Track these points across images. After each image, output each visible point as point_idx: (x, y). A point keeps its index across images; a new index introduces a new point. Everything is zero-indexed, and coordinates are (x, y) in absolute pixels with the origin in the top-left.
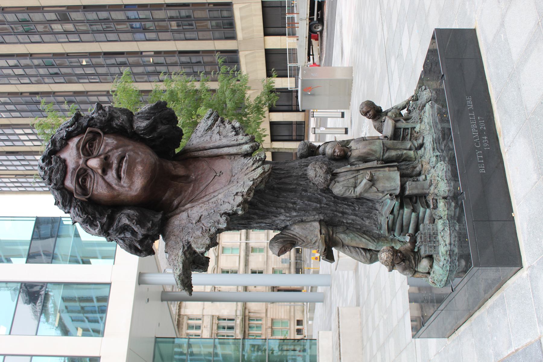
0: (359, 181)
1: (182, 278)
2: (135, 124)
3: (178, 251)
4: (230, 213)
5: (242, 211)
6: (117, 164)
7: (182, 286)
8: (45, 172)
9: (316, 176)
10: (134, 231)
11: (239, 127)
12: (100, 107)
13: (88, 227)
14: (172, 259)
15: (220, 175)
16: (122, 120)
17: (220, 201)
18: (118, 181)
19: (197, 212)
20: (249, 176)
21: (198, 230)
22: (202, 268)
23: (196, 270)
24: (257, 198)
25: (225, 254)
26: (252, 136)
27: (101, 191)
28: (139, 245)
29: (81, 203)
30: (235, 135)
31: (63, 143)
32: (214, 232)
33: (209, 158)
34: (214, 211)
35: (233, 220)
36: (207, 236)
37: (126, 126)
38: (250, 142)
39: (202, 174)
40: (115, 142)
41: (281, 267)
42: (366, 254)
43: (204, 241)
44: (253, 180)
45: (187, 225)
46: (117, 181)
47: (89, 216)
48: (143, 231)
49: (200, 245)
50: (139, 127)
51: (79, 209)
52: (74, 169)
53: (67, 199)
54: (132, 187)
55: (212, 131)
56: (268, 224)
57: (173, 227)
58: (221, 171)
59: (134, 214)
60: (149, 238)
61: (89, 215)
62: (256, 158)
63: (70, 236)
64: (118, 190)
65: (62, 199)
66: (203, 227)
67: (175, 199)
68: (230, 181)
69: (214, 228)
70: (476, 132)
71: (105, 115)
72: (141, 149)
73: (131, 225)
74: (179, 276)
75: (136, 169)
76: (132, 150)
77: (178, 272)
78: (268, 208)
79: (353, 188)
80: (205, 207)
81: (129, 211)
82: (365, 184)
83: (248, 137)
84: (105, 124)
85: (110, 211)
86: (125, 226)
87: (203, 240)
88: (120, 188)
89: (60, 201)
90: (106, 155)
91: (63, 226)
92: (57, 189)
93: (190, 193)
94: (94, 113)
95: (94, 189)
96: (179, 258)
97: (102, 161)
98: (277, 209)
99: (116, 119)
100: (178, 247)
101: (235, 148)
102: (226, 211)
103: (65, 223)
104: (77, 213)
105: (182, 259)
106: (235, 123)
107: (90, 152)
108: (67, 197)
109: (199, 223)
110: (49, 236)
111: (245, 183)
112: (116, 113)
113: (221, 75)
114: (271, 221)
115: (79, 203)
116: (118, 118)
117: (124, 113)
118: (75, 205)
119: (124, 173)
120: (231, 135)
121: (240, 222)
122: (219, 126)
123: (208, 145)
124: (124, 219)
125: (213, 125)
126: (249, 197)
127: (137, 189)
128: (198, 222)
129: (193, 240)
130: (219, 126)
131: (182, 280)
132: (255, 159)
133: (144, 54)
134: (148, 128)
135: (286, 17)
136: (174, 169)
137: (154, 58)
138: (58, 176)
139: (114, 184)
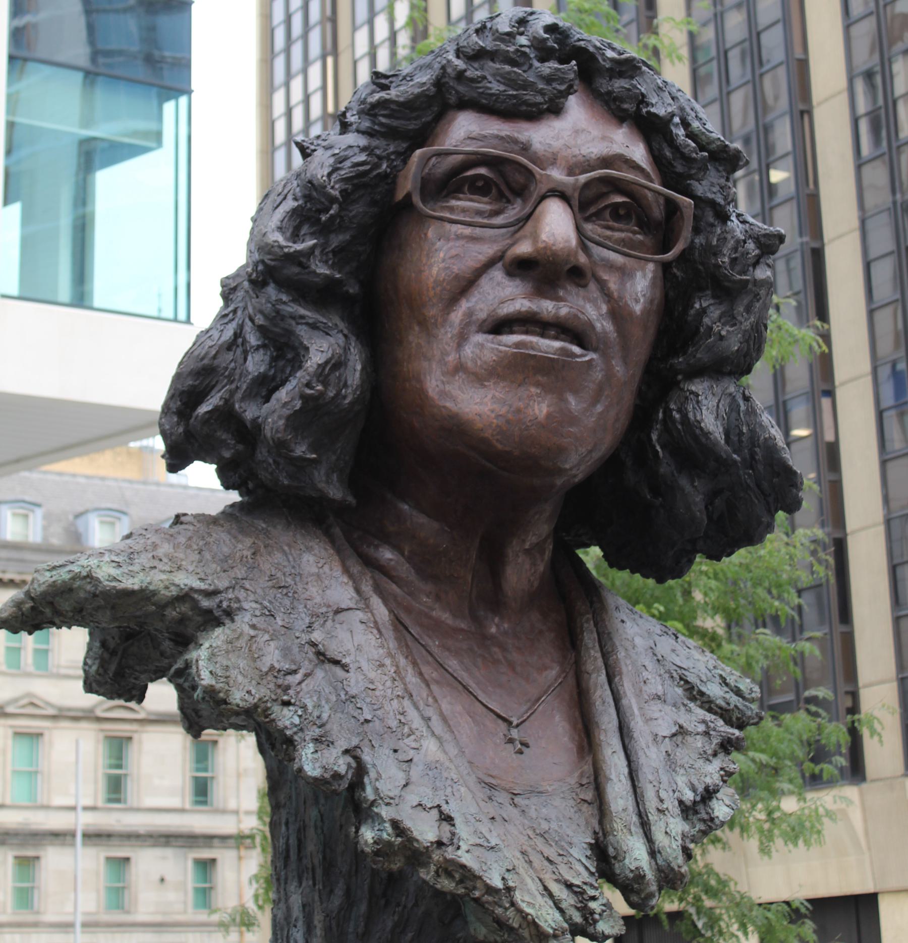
1: (80, 587)
2: (706, 384)
3: (191, 569)
4: (364, 789)
5: (375, 842)
6: (557, 317)
7: (43, 588)
10: (276, 389)
11: (712, 820)
12: (768, 246)
13: (290, 204)
14: (155, 546)
15: (511, 741)
16: (723, 333)
17: (414, 745)
18: (484, 321)
19: (359, 648)
20: (521, 871)
21: (286, 652)
22: (106, 671)
23: (98, 644)
25: (10, 742)
26: (683, 876)
27: (442, 255)
28: (216, 409)
30: (681, 802)
31: (626, 106)
32: (280, 724)
34: (367, 721)
35: (322, 801)
36: (261, 692)
37: (697, 351)
38: (659, 870)
39: (512, 666)
40: (638, 308)
43: (240, 678)
44: (509, 889)
45: (301, 608)
46: (482, 315)
48: (274, 422)
49: (225, 663)
50: (698, 402)
51: (361, 168)
52: (525, 148)
53: (403, 122)
54: (460, 377)
55: (686, 701)
57: (289, 546)
59: (345, 385)
60: (240, 447)
61: (340, 204)
62: (593, 898)
63: (87, 122)
64: (445, 321)
65: (401, 99)
66: (299, 677)
67: (403, 554)
68: (491, 787)
69: (297, 720)
71: (738, 268)
72: (613, 413)
73: (301, 376)
74: (89, 576)
75: (538, 395)
76: (609, 374)
77: (105, 572)
80: (384, 685)
81: (359, 367)
83: (680, 860)
84: (700, 267)
85: (353, 289)
86: (294, 348)
87: (245, 676)
89: (393, 94)
90: (589, 275)
91: (155, 102)
92: (439, 83)
93: (430, 617)
94: (744, 222)
95: (448, 226)
96: (163, 577)
97: (568, 255)
99: (723, 308)
100: (209, 571)
101: (630, 804)
102: (373, 774)
103: (169, 107)
104: (346, 159)
105: (162, 585)
107: (593, 210)
108: (409, 120)
109: (311, 655)
110: (100, 46)
111: (490, 856)
112: (748, 309)
113: (814, 726)
115: (384, 166)
116: (730, 318)
117: (747, 341)
118: (378, 152)
119: (518, 345)
120: (680, 783)
121: (311, 833)
122: (706, 734)
123: (627, 687)
124: (325, 346)
125: (708, 704)
126: (437, 872)
127: (454, 399)
128: (319, 654)
129: (241, 634)
130: (706, 734)
131: (71, 590)
132: (591, 892)
133: (826, 402)
134: (696, 438)
136: (527, 547)
137: (809, 443)
138: (496, 87)
139: (470, 305)
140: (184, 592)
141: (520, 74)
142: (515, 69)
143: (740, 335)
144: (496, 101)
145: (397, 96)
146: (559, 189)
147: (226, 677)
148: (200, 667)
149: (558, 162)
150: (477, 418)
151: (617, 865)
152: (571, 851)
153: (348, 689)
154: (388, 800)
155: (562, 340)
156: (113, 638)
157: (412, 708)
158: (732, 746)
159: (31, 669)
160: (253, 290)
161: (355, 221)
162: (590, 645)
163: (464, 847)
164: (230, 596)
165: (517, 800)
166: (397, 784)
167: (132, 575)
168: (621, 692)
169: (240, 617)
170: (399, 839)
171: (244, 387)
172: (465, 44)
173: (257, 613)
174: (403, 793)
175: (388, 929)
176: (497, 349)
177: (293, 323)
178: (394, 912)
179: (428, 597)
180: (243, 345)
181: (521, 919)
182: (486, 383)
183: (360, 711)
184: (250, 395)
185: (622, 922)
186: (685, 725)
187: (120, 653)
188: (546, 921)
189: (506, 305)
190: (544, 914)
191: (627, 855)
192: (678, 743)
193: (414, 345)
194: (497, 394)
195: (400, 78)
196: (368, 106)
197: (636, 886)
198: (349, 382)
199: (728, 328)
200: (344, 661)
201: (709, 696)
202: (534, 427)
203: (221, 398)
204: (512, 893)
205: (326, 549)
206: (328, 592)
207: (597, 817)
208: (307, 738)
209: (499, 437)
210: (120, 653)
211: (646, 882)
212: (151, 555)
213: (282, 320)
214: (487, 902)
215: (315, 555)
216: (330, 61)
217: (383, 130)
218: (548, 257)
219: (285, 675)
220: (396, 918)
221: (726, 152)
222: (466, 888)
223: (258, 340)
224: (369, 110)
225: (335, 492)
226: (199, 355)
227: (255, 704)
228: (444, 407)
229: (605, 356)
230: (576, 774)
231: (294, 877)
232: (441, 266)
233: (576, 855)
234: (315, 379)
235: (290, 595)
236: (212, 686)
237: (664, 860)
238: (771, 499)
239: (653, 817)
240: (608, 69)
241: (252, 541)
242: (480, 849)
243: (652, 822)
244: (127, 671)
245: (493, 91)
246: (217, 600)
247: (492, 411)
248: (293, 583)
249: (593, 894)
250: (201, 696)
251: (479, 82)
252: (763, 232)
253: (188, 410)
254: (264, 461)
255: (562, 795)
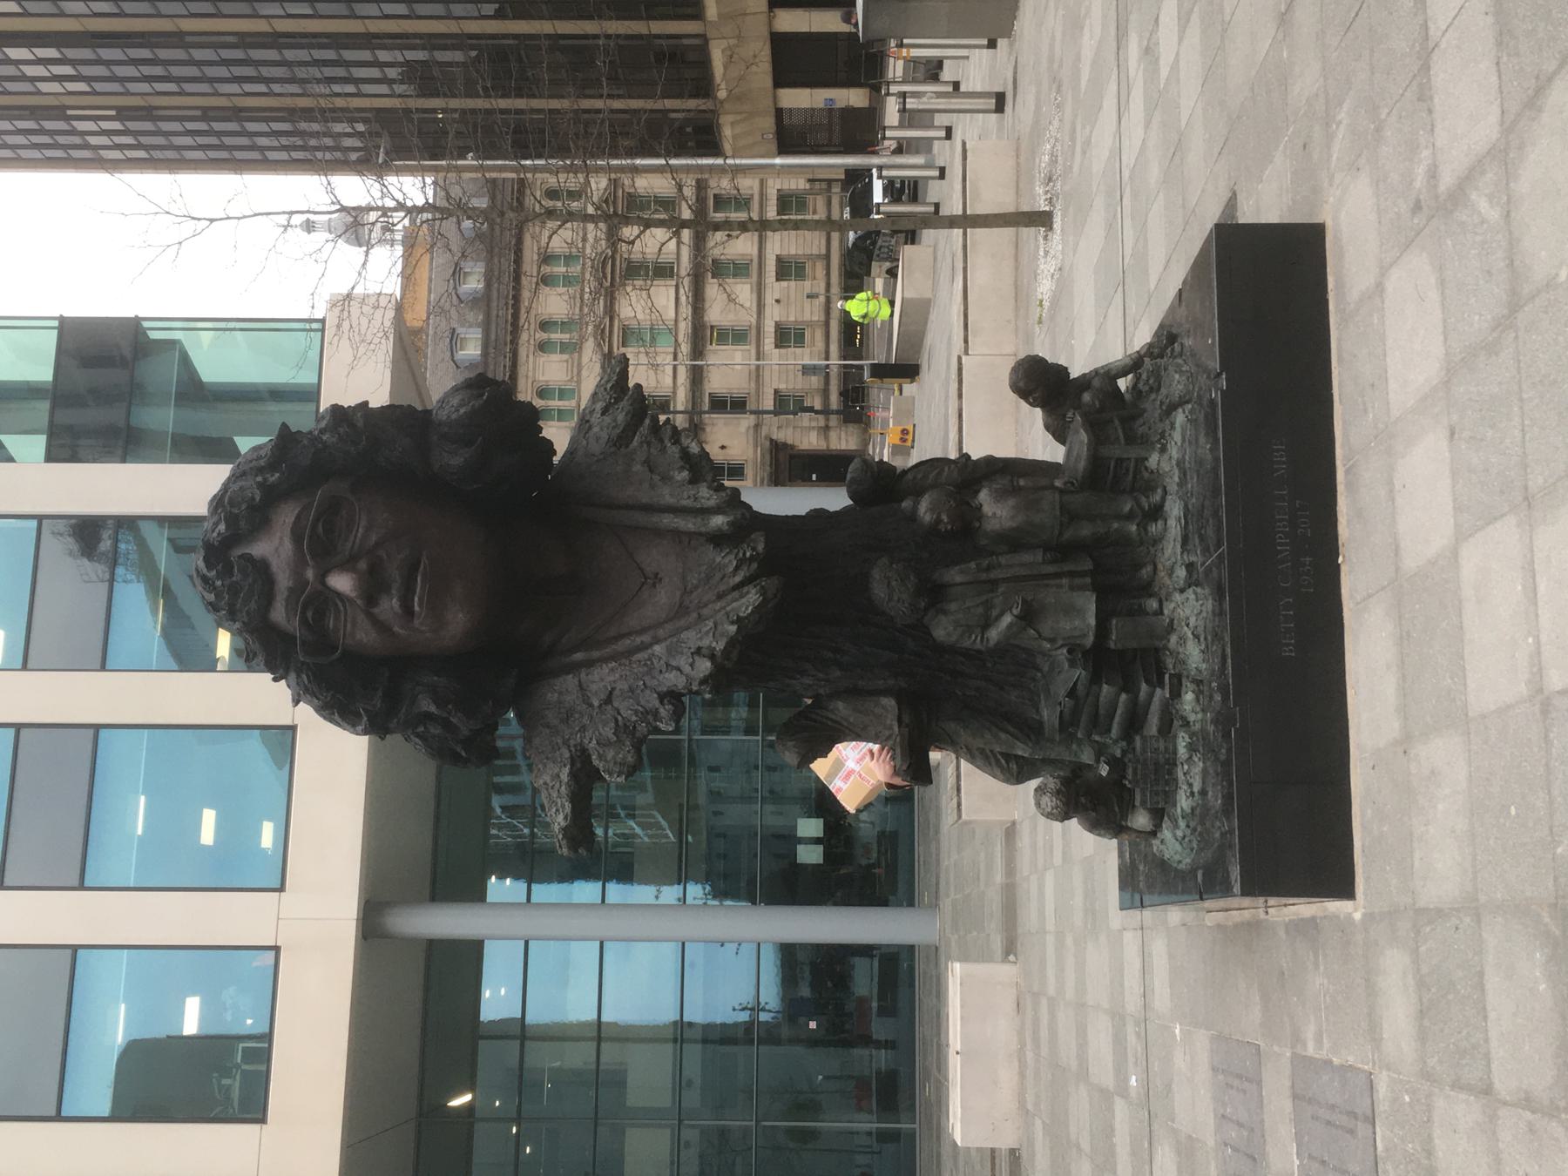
0: (995, 613)
9: (890, 600)
41: (799, 386)
42: (1008, 764)
58: (657, 574)
66: (620, 718)
70: (1286, 544)
79: (979, 630)
82: (1010, 626)
96: (563, 787)
106: (689, 441)
111: (720, 628)
119: (420, 605)
122: (649, 444)
132: (741, 555)
138: (253, 605)
159: (575, 335)
167: (563, 806)
216: (70, 112)
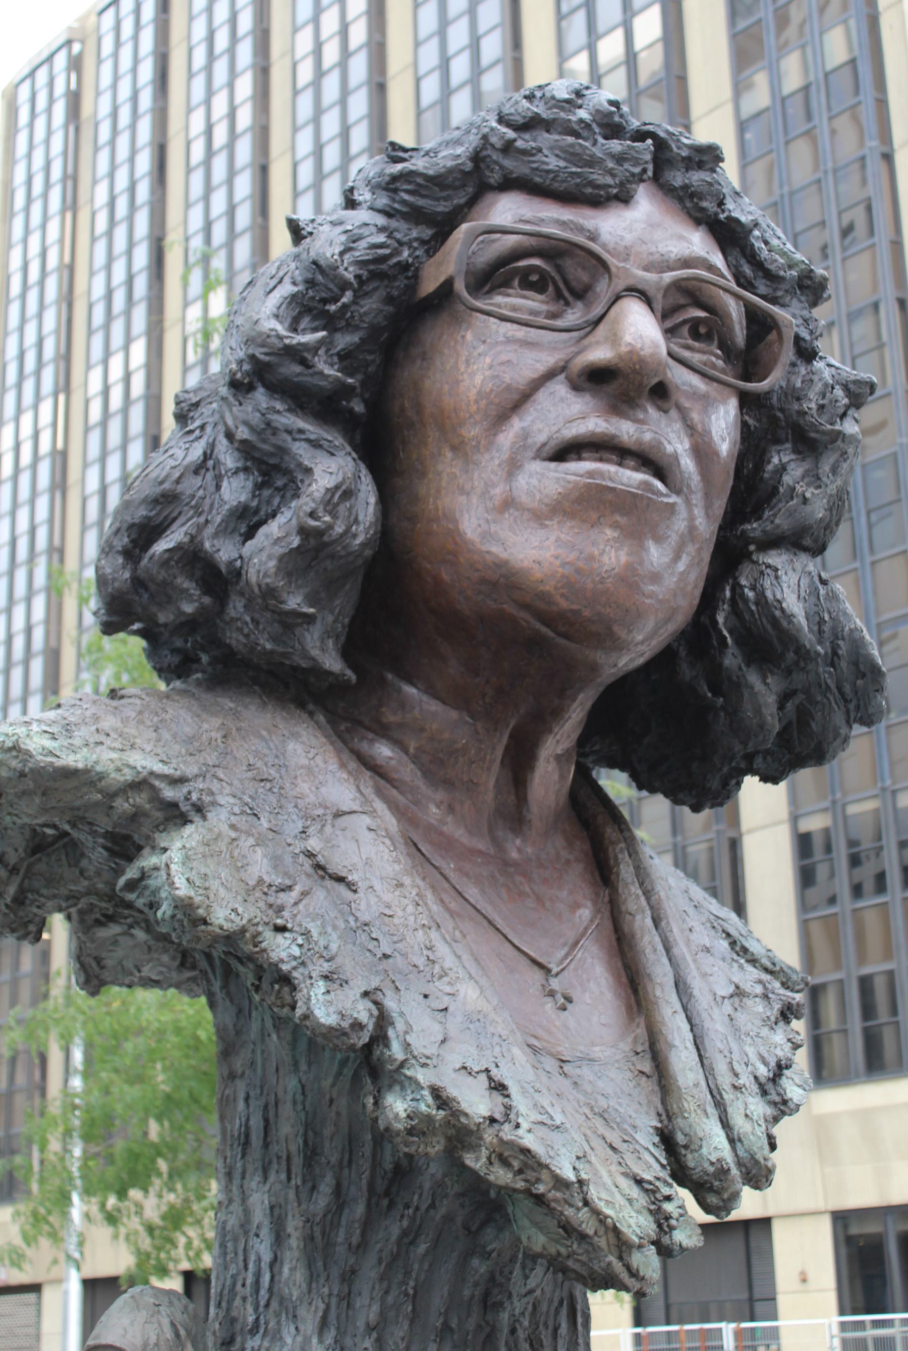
3: (148, 748)
4: (387, 1045)
5: (409, 1117)
6: (640, 442)
8: (568, 101)
13: (287, 289)
14: (96, 718)
15: (552, 994)
16: (808, 495)
17: (448, 989)
18: (544, 445)
21: (276, 862)
24: (442, 1211)
28: (178, 547)
29: (404, 267)
31: (705, 204)
32: (274, 956)
33: (613, 938)
34: (386, 956)
35: (303, 1067)
37: (775, 515)
43: (222, 892)
44: (581, 1182)
46: (541, 438)
47: (347, 297)
49: (203, 870)
50: (777, 577)
51: (381, 251)
54: (509, 517)
56: (266, 1278)
59: (356, 521)
60: (207, 600)
61: (355, 291)
64: (491, 444)
65: (431, 172)
66: (295, 894)
67: (406, 752)
69: (296, 951)
74: (15, 748)
78: (373, 1274)
84: (779, 414)
86: (287, 472)
88: (505, 455)
92: (477, 158)
93: (441, 833)
96: (114, 755)
98: (370, 1329)
99: (806, 465)
102: (400, 1025)
105: (112, 767)
108: (437, 199)
112: (834, 470)
114: (295, 1294)
115: (406, 254)
116: (815, 479)
118: (398, 235)
119: (591, 474)
120: (751, 1055)
121: (287, 1110)
124: (334, 468)
128: (318, 867)
129: (219, 835)
130: (766, 997)
132: (666, 1191)
134: (775, 622)
135: (722, 1325)
138: (553, 163)
140: (141, 776)
141: (586, 148)
142: (580, 141)
143: (825, 501)
144: (553, 179)
145: (425, 168)
146: (640, 287)
147: (206, 889)
148: (173, 873)
149: (632, 258)
150: (536, 566)
151: (689, 1157)
152: (638, 1137)
153: (358, 914)
154: (423, 1060)
155: (644, 472)
156: (16, 850)
157: (442, 942)
158: (792, 1013)
160: (234, 395)
161: (367, 320)
162: (629, 880)
163: (525, 1125)
164: (201, 786)
165: (567, 1068)
166: (433, 1039)
167: (73, 750)
168: (671, 939)
169: (213, 814)
170: (442, 1113)
171: (218, 519)
172: (512, 110)
173: (237, 810)
174: (441, 1052)
175: (394, 1238)
176: (564, 479)
177: (289, 438)
178: (402, 1216)
179: (438, 807)
180: (214, 468)
181: (597, 1224)
182: (547, 523)
183: (375, 943)
184: (224, 530)
185: (699, 1231)
186: (741, 984)
187: (22, 871)
188: (630, 1226)
189: (574, 424)
190: (627, 1216)
191: (704, 1143)
192: (736, 1006)
193: (445, 476)
194: (562, 536)
195: (422, 153)
196: (387, 179)
197: (716, 1183)
198: (361, 518)
199: (812, 489)
200: (350, 878)
201: (753, 954)
202: (610, 580)
203: (186, 534)
204: (585, 1188)
205: (315, 736)
206: (323, 790)
207: (659, 1095)
208: (314, 974)
209: (565, 591)
210: (22, 871)
211: (730, 1178)
212: (94, 728)
213: (274, 434)
214: (556, 1200)
215: (303, 743)
217: (405, 209)
218: (634, 364)
219: (277, 892)
220: (405, 1223)
221: (810, 278)
222: (526, 1181)
223: (237, 462)
224: (388, 183)
225: (332, 662)
226: (158, 477)
227: (244, 926)
228: (488, 552)
229: (688, 501)
230: (630, 1039)
231: (256, 1169)
232: (487, 373)
233: (642, 1142)
234: (321, 507)
235: (275, 790)
236: (190, 898)
237: (746, 1151)
238: (852, 706)
239: (728, 1096)
240: (683, 159)
241: (220, 721)
242: (544, 1128)
243: (728, 1102)
244: (30, 896)
245: (551, 167)
246: (185, 790)
247: (557, 557)
248: (278, 776)
249: (668, 1193)
250: (169, 913)
251: (533, 155)
252: (853, 378)
253: (137, 551)
254: (238, 619)
255: (617, 1065)
